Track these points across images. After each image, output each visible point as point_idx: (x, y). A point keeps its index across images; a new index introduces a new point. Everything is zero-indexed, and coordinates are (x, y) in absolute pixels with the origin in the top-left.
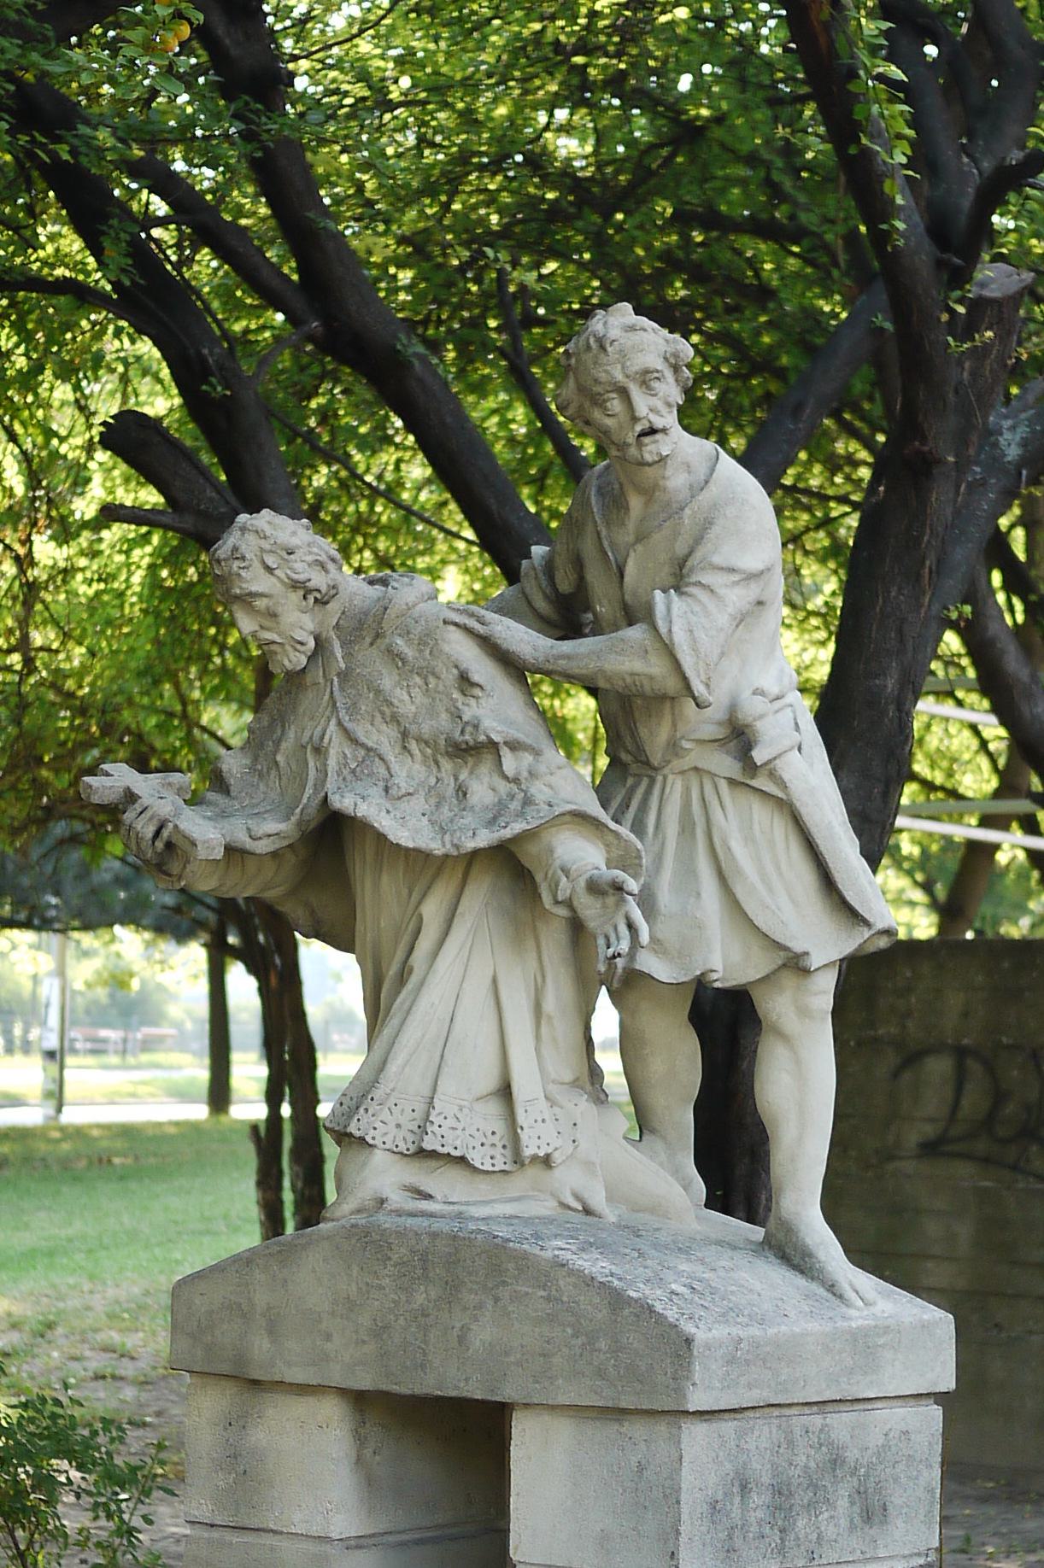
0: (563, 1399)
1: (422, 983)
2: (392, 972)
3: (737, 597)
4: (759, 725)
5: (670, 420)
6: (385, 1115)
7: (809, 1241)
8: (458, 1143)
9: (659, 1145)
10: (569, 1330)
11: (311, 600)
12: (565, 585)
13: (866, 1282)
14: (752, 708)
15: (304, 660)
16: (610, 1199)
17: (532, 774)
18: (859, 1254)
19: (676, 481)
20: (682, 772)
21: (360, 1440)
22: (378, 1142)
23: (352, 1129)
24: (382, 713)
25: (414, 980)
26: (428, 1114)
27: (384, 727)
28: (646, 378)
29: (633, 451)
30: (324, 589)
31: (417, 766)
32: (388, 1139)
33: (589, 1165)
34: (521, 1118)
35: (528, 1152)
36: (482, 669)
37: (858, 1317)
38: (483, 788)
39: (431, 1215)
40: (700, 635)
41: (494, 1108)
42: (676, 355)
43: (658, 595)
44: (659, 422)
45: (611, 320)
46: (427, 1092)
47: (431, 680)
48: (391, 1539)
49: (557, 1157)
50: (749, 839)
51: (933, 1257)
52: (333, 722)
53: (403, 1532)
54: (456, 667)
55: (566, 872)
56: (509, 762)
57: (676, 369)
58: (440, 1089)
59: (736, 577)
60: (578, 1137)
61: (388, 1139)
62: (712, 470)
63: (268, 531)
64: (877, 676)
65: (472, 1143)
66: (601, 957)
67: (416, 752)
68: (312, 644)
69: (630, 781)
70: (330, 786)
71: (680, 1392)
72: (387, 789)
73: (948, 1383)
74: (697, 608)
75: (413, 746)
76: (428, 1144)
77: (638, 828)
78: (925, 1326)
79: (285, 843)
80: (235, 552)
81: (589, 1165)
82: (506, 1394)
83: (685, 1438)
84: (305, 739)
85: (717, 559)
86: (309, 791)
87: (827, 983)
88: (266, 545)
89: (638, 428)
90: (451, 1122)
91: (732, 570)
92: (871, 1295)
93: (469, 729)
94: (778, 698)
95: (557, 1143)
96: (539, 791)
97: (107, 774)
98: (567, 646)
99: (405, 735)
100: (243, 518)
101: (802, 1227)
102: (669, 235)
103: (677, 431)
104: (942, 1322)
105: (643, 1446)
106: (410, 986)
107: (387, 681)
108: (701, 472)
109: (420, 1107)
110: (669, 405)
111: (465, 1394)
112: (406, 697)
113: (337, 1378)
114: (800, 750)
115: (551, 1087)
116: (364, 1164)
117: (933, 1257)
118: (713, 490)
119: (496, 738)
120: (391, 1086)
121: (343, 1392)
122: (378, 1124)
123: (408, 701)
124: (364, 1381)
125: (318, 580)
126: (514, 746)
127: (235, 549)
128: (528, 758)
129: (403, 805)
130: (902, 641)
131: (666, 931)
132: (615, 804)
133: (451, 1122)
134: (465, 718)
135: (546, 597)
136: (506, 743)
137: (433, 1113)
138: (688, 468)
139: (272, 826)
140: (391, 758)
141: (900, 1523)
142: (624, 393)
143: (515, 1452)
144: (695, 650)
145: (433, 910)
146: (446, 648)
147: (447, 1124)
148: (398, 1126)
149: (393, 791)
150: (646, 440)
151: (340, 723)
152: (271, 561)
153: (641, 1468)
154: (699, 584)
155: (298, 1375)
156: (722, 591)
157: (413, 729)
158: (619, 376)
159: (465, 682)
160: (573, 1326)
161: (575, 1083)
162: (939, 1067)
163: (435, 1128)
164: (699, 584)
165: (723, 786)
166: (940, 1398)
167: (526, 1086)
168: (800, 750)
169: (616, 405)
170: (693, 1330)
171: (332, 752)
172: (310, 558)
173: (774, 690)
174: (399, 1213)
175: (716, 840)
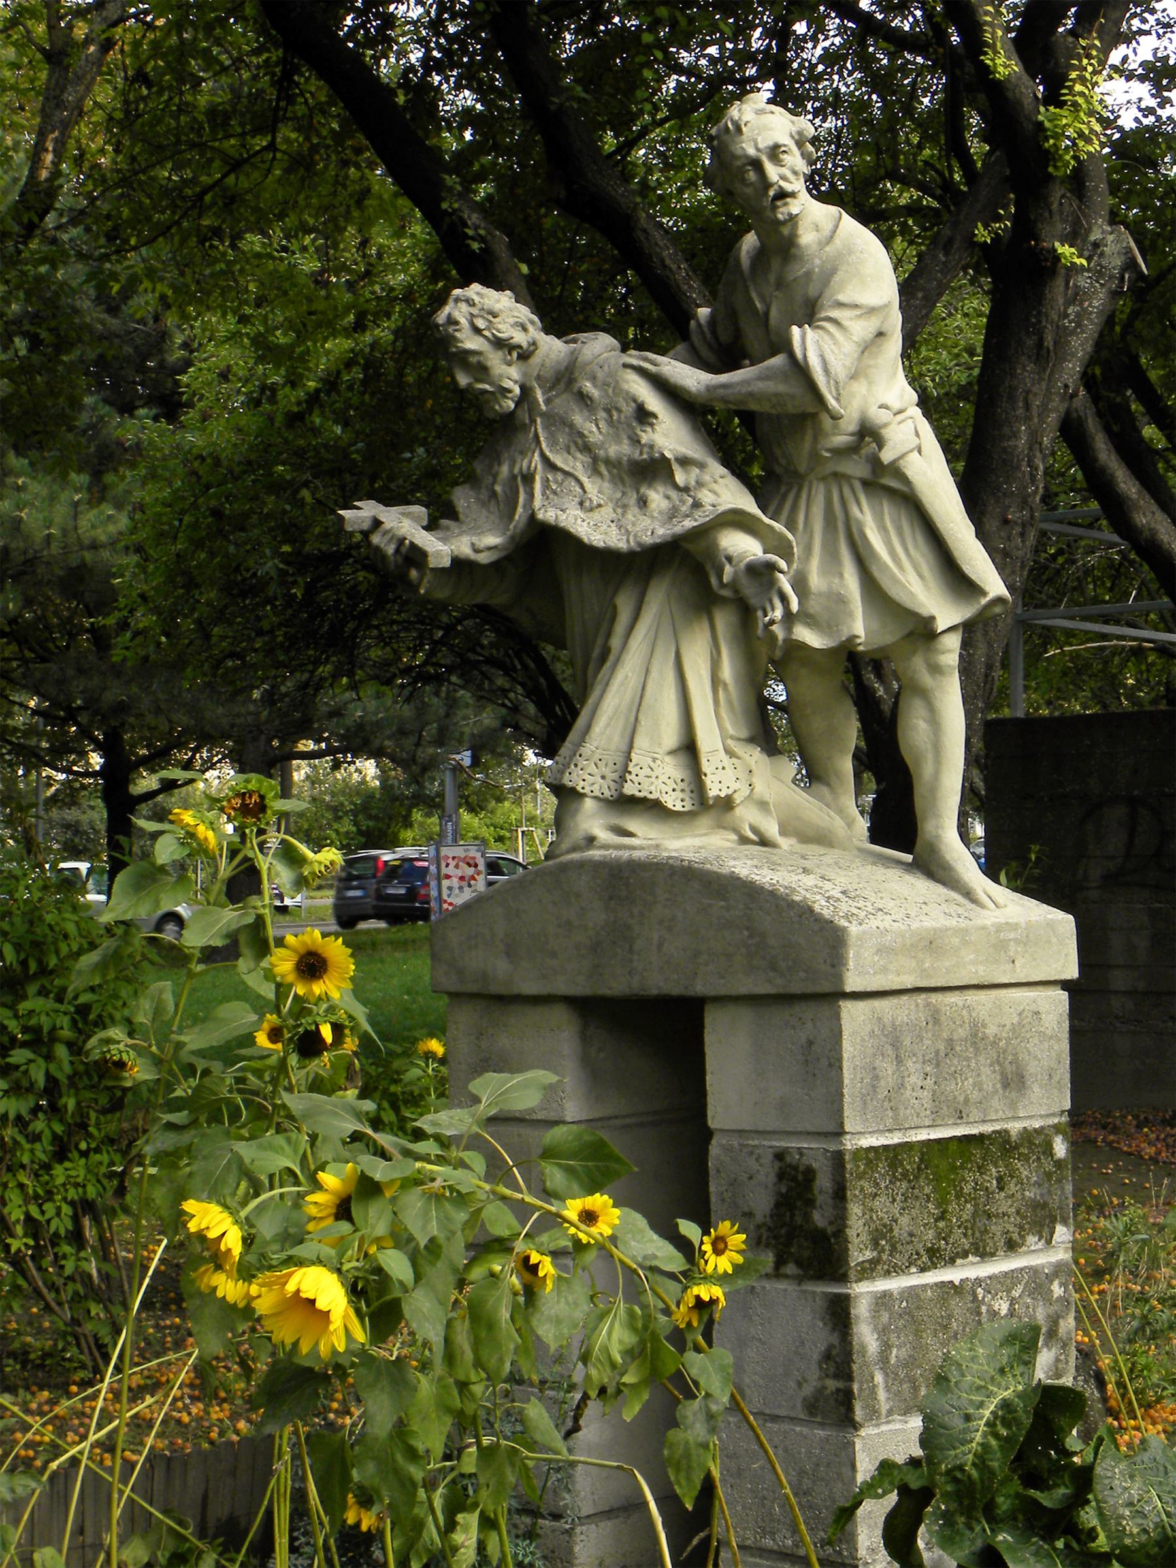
0: (743, 990)
1: (618, 660)
2: (596, 652)
3: (861, 329)
4: (884, 432)
5: (797, 185)
6: (592, 768)
7: (948, 857)
8: (652, 788)
9: (825, 790)
10: (746, 933)
11: (515, 355)
12: (725, 338)
13: (1000, 892)
14: (879, 416)
15: (512, 406)
16: (783, 832)
17: (700, 484)
18: (991, 870)
19: (807, 238)
20: (823, 479)
21: (584, 1038)
22: (587, 791)
23: (566, 781)
24: (576, 443)
25: (611, 658)
26: (627, 766)
27: (579, 455)
28: (775, 152)
29: (768, 213)
30: (525, 345)
31: (606, 484)
32: (596, 788)
33: (763, 805)
34: (706, 767)
35: (712, 793)
36: (653, 402)
37: (989, 917)
38: (657, 497)
39: (633, 848)
40: (831, 358)
41: (682, 758)
42: (800, 133)
43: (795, 330)
44: (788, 187)
45: (744, 106)
46: (624, 748)
47: (615, 413)
48: (618, 1122)
49: (738, 798)
50: (882, 528)
51: (1118, 966)
52: (537, 456)
53: (624, 1117)
54: (635, 401)
55: (729, 559)
56: (680, 477)
57: (800, 144)
58: (636, 745)
59: (858, 312)
60: (754, 780)
61: (596, 788)
62: (836, 227)
63: (477, 299)
64: (1010, 438)
65: (664, 788)
66: (761, 625)
67: (605, 473)
68: (517, 390)
69: (783, 489)
70: (538, 501)
71: (839, 978)
72: (581, 504)
73: (1072, 972)
74: (826, 337)
75: (603, 469)
76: (629, 789)
77: (791, 525)
78: (1051, 925)
79: (503, 554)
80: (452, 321)
81: (763, 805)
82: (700, 988)
83: (844, 1015)
84: (516, 471)
85: (841, 298)
86: (520, 510)
87: (952, 644)
88: (475, 311)
89: (771, 193)
90: (647, 771)
91: (856, 306)
92: (1000, 900)
93: (646, 450)
94: (900, 412)
95: (737, 786)
96: (706, 497)
97: (358, 508)
98: (724, 378)
99: (595, 459)
100: (457, 292)
101: (943, 847)
102: (1019, 431)
103: (804, 196)
104: (1064, 922)
105: (809, 1024)
106: (608, 664)
107: (578, 419)
108: (827, 227)
109: (620, 760)
110: (795, 173)
111: (665, 992)
112: (594, 429)
113: (562, 987)
114: (920, 452)
115: (730, 742)
116: (577, 811)
117: (1118, 966)
118: (838, 242)
119: (668, 455)
120: (595, 744)
121: (571, 1001)
122: (587, 777)
123: (593, 430)
124: (580, 987)
125: (519, 338)
126: (684, 462)
127: (449, 316)
128: (695, 471)
129: (596, 515)
130: (1027, 407)
131: (814, 606)
132: (772, 508)
133: (647, 771)
134: (643, 441)
135: (710, 347)
136: (677, 459)
137: (631, 765)
138: (817, 228)
139: (492, 540)
140: (585, 480)
141: (1036, 1088)
142: (757, 165)
143: (709, 1038)
144: (826, 371)
145: (624, 604)
146: (625, 387)
147: (642, 773)
148: (603, 777)
149: (587, 504)
150: (779, 203)
151: (543, 456)
152: (480, 324)
153: (810, 1043)
154: (829, 319)
155: (530, 988)
156: (845, 323)
157: (602, 453)
158: (751, 151)
159: (644, 416)
160: (747, 928)
161: (751, 740)
162: (1118, 813)
163: (633, 777)
164: (829, 319)
165: (858, 485)
166: (1065, 985)
167: (708, 739)
168: (920, 452)
169: (752, 176)
170: (846, 924)
171: (538, 478)
172: (512, 320)
173: (896, 405)
174: (606, 847)
175: (854, 530)
